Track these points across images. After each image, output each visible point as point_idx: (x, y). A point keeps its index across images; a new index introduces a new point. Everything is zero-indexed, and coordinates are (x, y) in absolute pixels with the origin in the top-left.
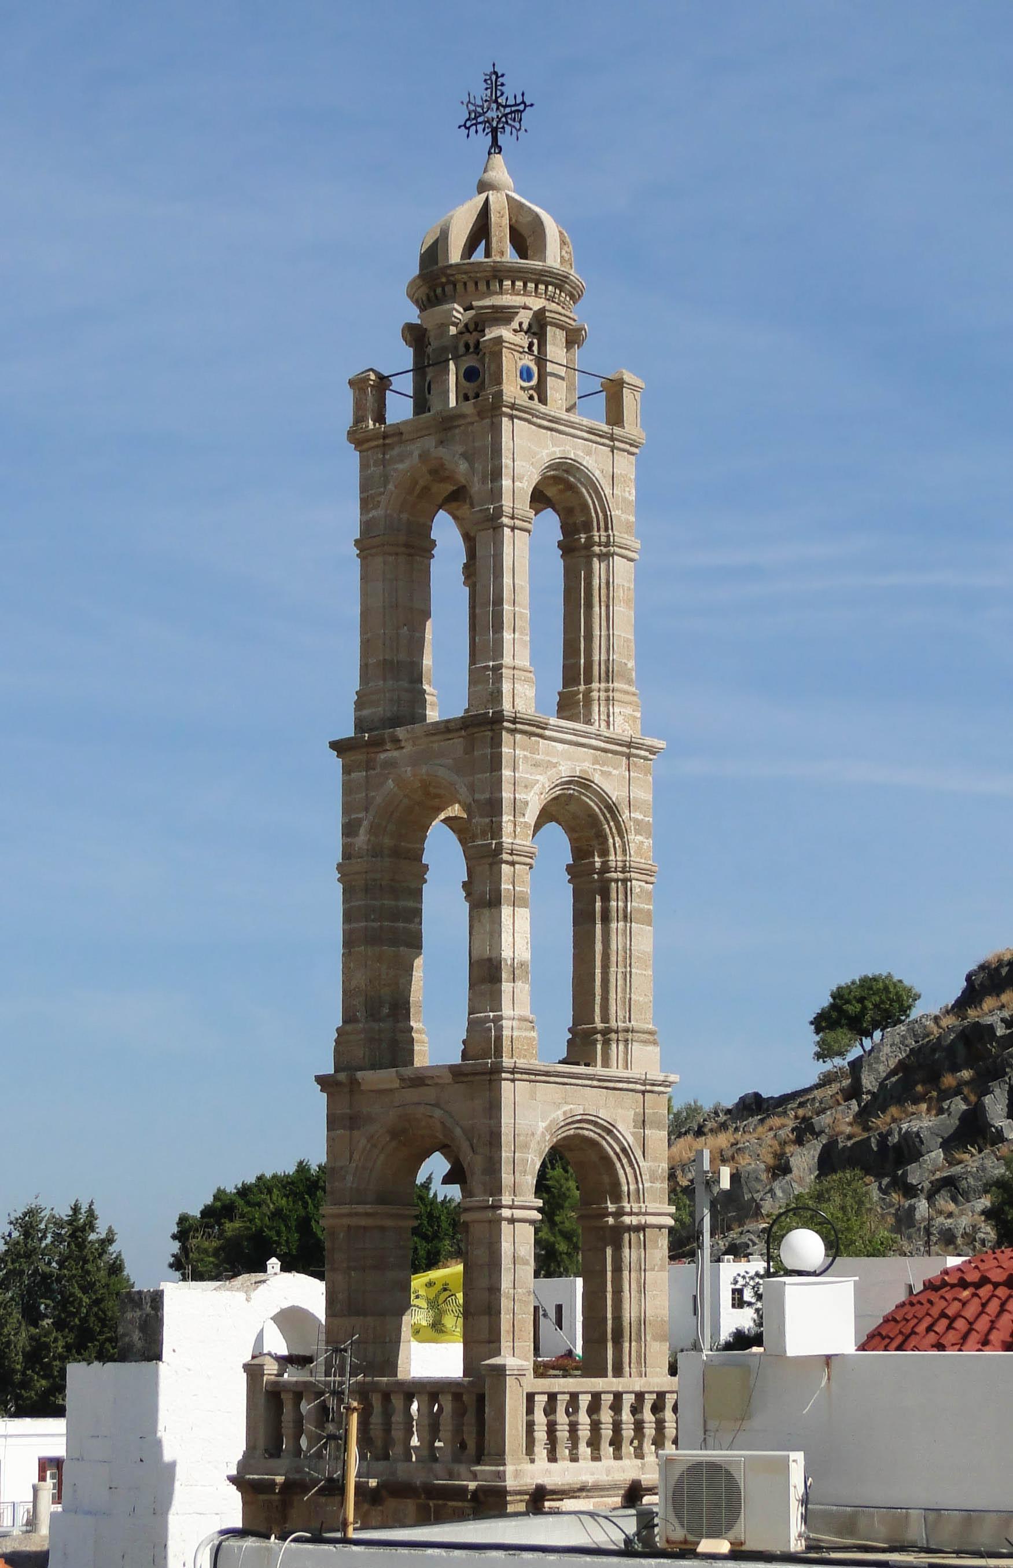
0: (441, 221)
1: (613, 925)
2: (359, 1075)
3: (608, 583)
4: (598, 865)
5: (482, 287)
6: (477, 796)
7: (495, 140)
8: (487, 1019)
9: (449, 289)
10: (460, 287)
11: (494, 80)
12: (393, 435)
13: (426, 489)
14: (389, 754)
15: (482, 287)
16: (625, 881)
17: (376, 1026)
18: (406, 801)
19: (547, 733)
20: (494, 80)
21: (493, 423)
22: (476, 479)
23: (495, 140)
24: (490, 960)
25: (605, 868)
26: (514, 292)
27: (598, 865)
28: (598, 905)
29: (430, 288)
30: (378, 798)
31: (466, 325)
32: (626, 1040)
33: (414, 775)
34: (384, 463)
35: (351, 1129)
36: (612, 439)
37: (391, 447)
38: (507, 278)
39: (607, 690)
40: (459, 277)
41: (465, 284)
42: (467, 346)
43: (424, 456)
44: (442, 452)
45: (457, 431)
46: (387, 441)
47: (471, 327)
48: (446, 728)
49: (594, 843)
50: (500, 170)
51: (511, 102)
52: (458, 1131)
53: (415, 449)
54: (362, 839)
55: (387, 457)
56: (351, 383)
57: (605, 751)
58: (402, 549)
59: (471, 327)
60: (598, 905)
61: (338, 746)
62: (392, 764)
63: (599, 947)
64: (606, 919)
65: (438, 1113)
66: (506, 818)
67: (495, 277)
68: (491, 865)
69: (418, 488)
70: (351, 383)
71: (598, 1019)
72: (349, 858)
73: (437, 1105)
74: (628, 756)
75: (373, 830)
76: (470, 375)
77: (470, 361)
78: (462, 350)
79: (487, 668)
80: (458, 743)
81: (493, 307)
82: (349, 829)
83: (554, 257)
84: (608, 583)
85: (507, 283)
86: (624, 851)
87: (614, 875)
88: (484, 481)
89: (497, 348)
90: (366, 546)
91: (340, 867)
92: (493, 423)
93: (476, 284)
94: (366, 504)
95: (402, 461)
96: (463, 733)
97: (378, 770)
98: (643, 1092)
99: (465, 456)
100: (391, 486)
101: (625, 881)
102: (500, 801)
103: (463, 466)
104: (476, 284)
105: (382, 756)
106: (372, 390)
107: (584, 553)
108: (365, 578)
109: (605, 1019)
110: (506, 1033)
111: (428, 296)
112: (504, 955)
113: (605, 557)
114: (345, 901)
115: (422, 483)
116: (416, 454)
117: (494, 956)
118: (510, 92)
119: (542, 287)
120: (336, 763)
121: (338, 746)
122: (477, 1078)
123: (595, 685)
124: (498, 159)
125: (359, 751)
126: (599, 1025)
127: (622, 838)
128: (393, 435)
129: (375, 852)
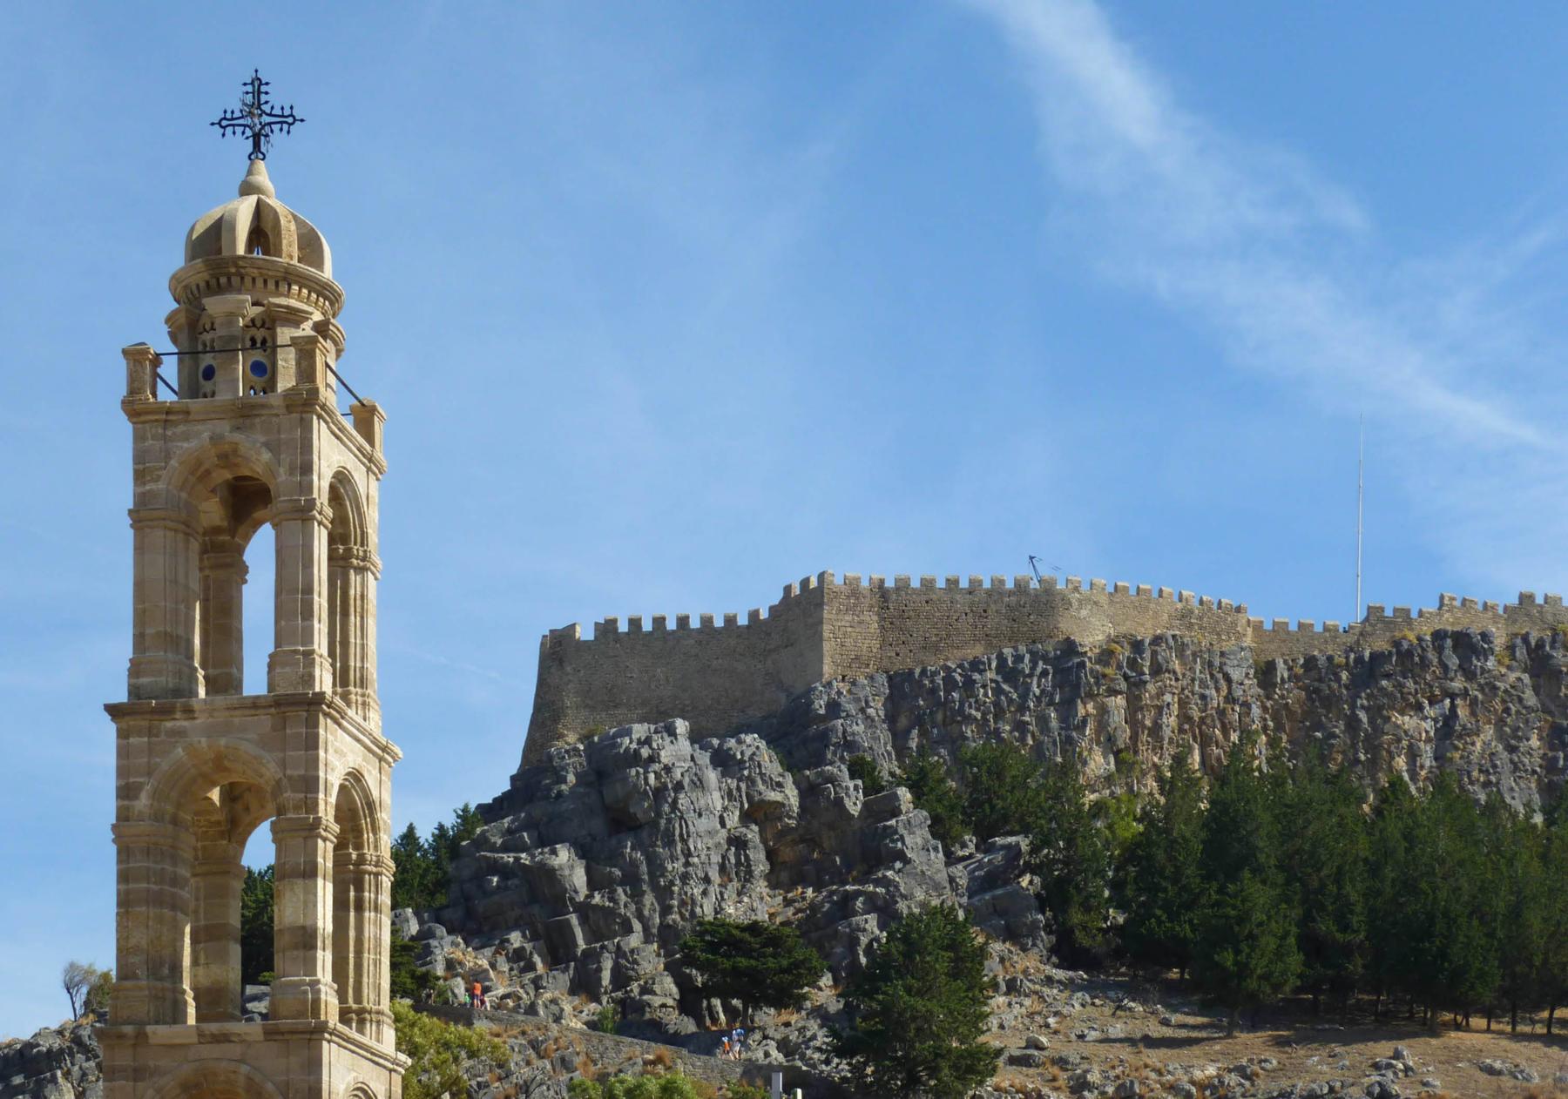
0: (216, 213)
1: (367, 914)
2: (149, 1029)
3: (362, 596)
4: (354, 857)
5: (271, 285)
6: (289, 772)
7: (257, 146)
8: (303, 983)
9: (235, 281)
10: (248, 281)
11: (257, 86)
12: (178, 413)
13: (208, 472)
14: (178, 723)
15: (271, 285)
16: (377, 875)
17: (159, 984)
18: (193, 771)
19: (345, 723)
20: (257, 86)
21: (302, 419)
22: (282, 470)
23: (257, 146)
24: (303, 928)
25: (362, 860)
26: (299, 297)
27: (354, 857)
28: (352, 894)
29: (212, 276)
30: (165, 765)
31: (253, 320)
32: (378, 1022)
33: (210, 747)
34: (165, 438)
35: (135, 1080)
36: (370, 461)
37: (175, 424)
38: (296, 283)
39: (363, 695)
40: (249, 270)
41: (254, 280)
42: (253, 340)
43: (216, 439)
44: (237, 437)
45: (257, 420)
46: (171, 417)
47: (258, 324)
48: (255, 704)
49: (350, 837)
50: (263, 176)
51: (277, 111)
52: (270, 1086)
53: (205, 433)
54: (143, 802)
55: (169, 433)
56: (125, 352)
57: (370, 750)
58: (182, 527)
59: (258, 324)
60: (352, 894)
61: (114, 711)
62: (181, 733)
63: (352, 933)
64: (359, 908)
65: (244, 1069)
66: (321, 796)
67: (285, 279)
68: (305, 838)
69: (202, 469)
70: (125, 352)
71: (351, 1000)
72: (127, 819)
73: (242, 1061)
74: (381, 759)
75: (156, 795)
76: (258, 368)
77: (258, 356)
78: (248, 344)
79: (296, 652)
80: (265, 721)
81: (287, 307)
82: (126, 792)
83: (328, 273)
84: (362, 596)
85: (295, 288)
86: (376, 847)
87: (369, 868)
88: (292, 471)
89: (309, 347)
90: (141, 516)
91: (114, 828)
92: (302, 419)
93: (265, 282)
94: (140, 476)
95: (187, 439)
96: (273, 710)
97: (163, 737)
98: (391, 1071)
99: (267, 445)
100: (173, 462)
101: (377, 875)
102: (317, 778)
103: (266, 456)
104: (265, 282)
105: (169, 724)
106: (140, 360)
107: (341, 563)
108: (140, 549)
109: (358, 999)
110: (323, 996)
111: (207, 283)
112: (320, 924)
113: (362, 570)
114: (119, 862)
115: (206, 466)
116: (206, 435)
117: (309, 923)
118: (276, 98)
119: (314, 296)
120: (109, 729)
121: (114, 711)
122: (295, 1037)
123: (352, 688)
124: (261, 165)
125: (142, 713)
126: (355, 1006)
127: (375, 834)
128: (178, 413)
129: (157, 817)
